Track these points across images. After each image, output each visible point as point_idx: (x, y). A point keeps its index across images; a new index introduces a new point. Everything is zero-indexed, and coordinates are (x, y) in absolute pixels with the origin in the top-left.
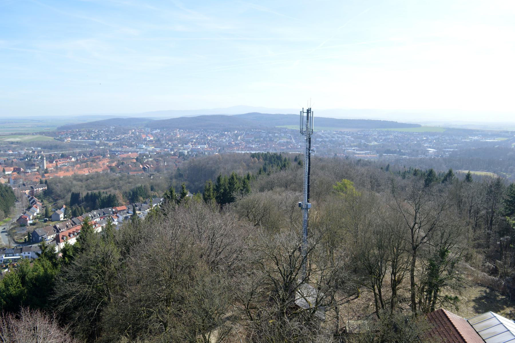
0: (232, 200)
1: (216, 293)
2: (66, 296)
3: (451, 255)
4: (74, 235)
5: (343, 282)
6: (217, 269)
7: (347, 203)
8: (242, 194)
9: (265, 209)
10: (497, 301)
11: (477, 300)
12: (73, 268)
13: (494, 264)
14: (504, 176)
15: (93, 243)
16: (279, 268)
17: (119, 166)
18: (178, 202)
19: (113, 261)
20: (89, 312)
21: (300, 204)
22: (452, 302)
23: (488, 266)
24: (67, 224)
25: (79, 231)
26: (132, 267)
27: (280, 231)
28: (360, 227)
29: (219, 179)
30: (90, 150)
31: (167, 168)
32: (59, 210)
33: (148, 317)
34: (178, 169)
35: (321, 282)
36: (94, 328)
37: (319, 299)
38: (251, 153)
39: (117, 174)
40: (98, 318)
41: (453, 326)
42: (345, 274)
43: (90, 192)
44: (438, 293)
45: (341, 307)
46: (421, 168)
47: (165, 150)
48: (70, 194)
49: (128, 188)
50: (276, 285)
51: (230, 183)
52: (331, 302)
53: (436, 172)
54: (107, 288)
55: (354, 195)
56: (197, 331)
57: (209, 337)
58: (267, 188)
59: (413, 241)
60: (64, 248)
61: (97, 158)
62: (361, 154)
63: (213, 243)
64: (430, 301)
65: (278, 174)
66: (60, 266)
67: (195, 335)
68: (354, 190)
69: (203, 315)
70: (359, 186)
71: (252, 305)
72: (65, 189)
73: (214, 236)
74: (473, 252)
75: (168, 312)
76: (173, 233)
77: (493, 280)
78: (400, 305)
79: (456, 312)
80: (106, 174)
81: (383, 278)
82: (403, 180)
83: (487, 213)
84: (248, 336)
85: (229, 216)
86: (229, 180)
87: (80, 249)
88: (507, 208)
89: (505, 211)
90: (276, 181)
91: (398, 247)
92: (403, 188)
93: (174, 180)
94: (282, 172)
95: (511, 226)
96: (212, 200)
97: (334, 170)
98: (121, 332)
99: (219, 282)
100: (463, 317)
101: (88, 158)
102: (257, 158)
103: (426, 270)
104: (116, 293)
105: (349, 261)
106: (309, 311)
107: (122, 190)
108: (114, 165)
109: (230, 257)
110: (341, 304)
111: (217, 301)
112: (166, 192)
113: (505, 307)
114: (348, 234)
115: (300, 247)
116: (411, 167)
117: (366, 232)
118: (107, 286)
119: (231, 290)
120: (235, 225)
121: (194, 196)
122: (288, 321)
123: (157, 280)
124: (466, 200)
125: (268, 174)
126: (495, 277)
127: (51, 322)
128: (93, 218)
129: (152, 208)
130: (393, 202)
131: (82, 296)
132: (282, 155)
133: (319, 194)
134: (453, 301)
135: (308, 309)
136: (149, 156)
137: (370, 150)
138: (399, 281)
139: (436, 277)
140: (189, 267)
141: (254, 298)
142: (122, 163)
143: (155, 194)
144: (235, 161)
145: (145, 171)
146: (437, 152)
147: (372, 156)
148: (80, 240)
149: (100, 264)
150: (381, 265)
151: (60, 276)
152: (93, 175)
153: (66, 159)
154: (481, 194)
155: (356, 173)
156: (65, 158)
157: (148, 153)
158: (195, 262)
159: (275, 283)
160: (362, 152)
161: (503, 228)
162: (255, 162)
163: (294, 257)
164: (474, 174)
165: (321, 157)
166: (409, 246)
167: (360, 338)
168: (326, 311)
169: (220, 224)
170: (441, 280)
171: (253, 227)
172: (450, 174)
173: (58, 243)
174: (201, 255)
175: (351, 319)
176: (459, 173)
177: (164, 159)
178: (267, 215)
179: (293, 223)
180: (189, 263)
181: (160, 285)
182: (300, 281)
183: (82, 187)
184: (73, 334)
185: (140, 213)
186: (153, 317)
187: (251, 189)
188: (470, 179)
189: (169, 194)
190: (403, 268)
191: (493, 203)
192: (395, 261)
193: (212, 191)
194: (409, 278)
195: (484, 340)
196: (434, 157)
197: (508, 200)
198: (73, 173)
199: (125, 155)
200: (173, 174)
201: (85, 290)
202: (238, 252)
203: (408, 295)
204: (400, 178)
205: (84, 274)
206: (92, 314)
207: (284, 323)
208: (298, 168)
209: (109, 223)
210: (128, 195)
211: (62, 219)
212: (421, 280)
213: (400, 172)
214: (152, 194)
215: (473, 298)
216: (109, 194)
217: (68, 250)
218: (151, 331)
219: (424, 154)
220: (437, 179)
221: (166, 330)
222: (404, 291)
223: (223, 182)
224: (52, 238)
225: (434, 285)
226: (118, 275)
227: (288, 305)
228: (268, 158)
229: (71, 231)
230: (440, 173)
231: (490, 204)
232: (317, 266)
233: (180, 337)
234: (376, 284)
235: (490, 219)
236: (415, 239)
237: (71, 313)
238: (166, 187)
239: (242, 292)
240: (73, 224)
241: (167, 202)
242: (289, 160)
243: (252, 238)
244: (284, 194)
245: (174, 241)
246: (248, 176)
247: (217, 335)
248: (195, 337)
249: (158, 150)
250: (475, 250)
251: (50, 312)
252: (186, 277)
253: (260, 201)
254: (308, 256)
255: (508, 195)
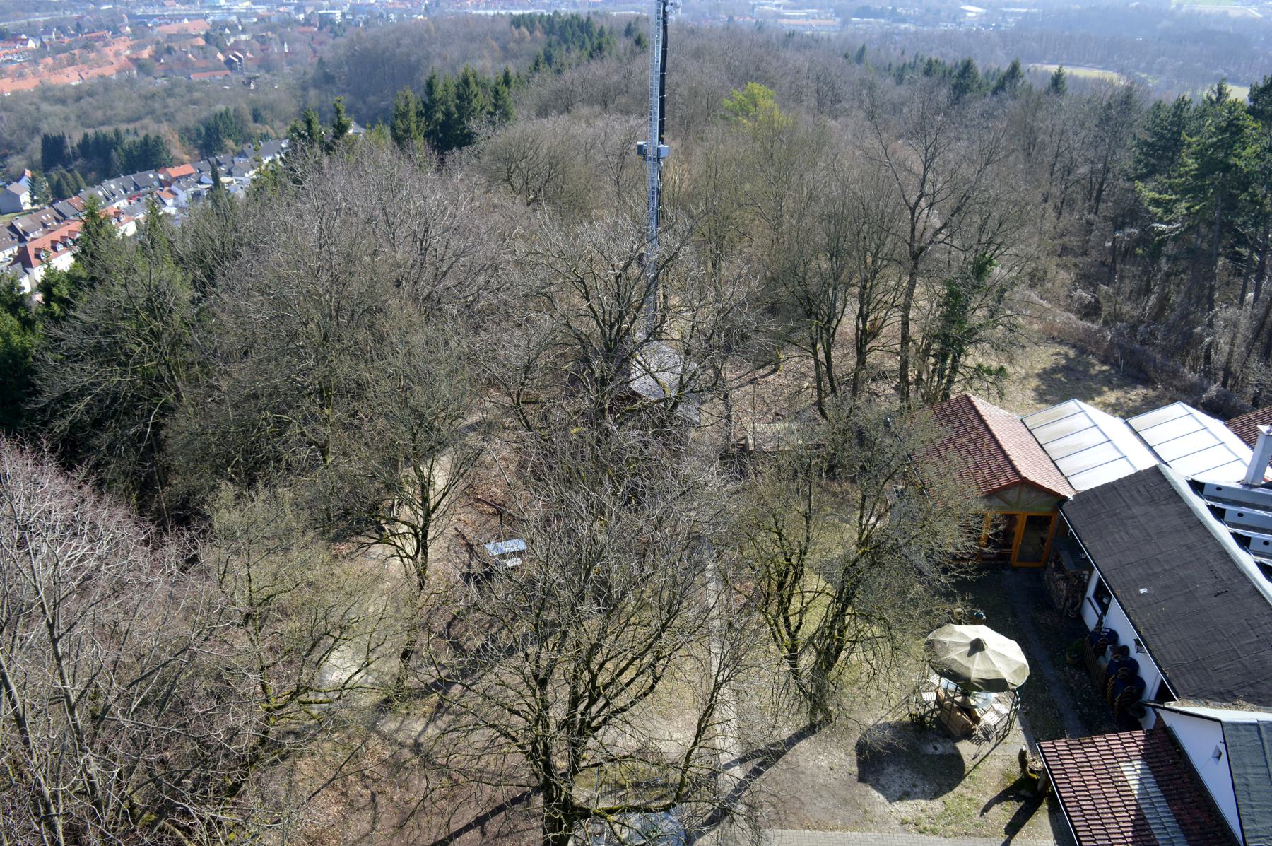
0: (466, 139)
1: (441, 371)
2: (67, 398)
3: (997, 272)
4: (65, 245)
5: (744, 337)
6: (439, 314)
7: (758, 144)
8: (493, 123)
9: (553, 162)
10: (1090, 375)
11: (1045, 375)
12: (75, 328)
13: (1094, 292)
14: (1144, 82)
15: (116, 262)
16: (590, 306)
17: (160, 57)
18: (329, 149)
19: (176, 305)
20: (133, 430)
21: (640, 147)
22: (991, 379)
23: (1080, 298)
24: (44, 217)
25: (78, 235)
26: (224, 317)
27: (590, 216)
28: (789, 203)
29: (430, 86)
30: (75, 15)
31: (291, 58)
32: (14, 183)
33: (280, 434)
34: (321, 62)
35: (691, 337)
36: (151, 466)
37: (686, 377)
38: (511, 14)
39: (159, 81)
40: (157, 444)
41: (990, 432)
42: (748, 317)
43: (91, 132)
44: (962, 359)
45: (736, 394)
46: (942, 55)
47: (281, 9)
48: (37, 143)
49: (192, 116)
50: (584, 347)
51: (459, 97)
52: (716, 383)
53: (979, 67)
54: (170, 371)
55: (776, 125)
56: (401, 459)
57: (430, 472)
58: (555, 108)
59: (913, 237)
60: (44, 281)
61: (99, 38)
62: (794, 17)
63: (426, 249)
64: (941, 376)
65: (582, 69)
66: (41, 326)
67: (396, 470)
68: (776, 112)
69: (411, 422)
70: (786, 103)
71: (528, 394)
72: (23, 126)
73: (426, 231)
74: (1051, 264)
75: (326, 420)
76: (321, 228)
77: (1087, 330)
78: (873, 386)
79: (998, 400)
80: (127, 80)
81: (837, 326)
82: (898, 88)
83: (1092, 172)
84: (522, 465)
85: (462, 180)
86: (458, 87)
87: (85, 279)
88: (1139, 161)
89: (1136, 169)
90: (579, 89)
91: (877, 253)
92: (896, 109)
93: (312, 93)
94: (594, 65)
95: (1142, 205)
96: (415, 142)
97: (727, 59)
98: (218, 471)
99: (447, 343)
100: (1012, 411)
101: (72, 39)
102: (527, 27)
103: (939, 306)
104: (193, 381)
105: (759, 286)
106: (662, 405)
107: (177, 122)
108: (145, 54)
109: (470, 283)
110: (737, 388)
111: (444, 389)
112: (293, 123)
113: (1105, 389)
114: (756, 222)
115: (642, 254)
116: (920, 54)
117: (802, 216)
118: (168, 366)
119: (476, 362)
120: (477, 204)
121: (368, 131)
122: (615, 428)
123: (291, 346)
124: (1047, 138)
125: (559, 72)
126: (1093, 322)
127: (38, 462)
128: (108, 199)
129: (263, 168)
130: (871, 142)
131: (108, 394)
132: (593, 19)
133: (686, 123)
134: (993, 377)
135: (661, 401)
136: (240, 28)
137: (820, 8)
138: (874, 334)
139: (960, 322)
140: (372, 311)
141: (533, 379)
142: (169, 50)
143: (264, 131)
144: (471, 38)
145: (231, 69)
146: (986, 14)
147: (823, 22)
148: (82, 256)
149: (143, 315)
150: (835, 295)
151: (46, 349)
152: (91, 85)
153: (12, 44)
154: (1082, 125)
155: (781, 67)
156: (9, 40)
157: (234, 18)
158: (382, 298)
159: (582, 341)
160: (797, 13)
161: (1123, 209)
162: (522, 39)
163: (627, 278)
164: (1071, 74)
165: (694, 24)
166: (903, 251)
167: (781, 462)
168: (703, 403)
169: (440, 202)
170: (969, 331)
171: (522, 209)
172: (1014, 72)
173: (28, 269)
174: (398, 281)
175: (759, 420)
176: (1036, 71)
177: (280, 36)
178: (556, 176)
179: (624, 195)
180: (369, 302)
181: (301, 359)
182: (640, 336)
183: (66, 119)
184: (100, 483)
185: (232, 182)
186: (293, 432)
187: (514, 111)
188: (1060, 86)
189: (302, 127)
190: (886, 303)
191: (1109, 148)
192: (868, 285)
193: (414, 118)
194: (898, 325)
195: (1053, 462)
196: (978, 29)
197: (1145, 143)
198: (36, 82)
199: (173, 28)
200: (309, 76)
201: (116, 379)
202: (489, 271)
203: (892, 364)
204: (890, 81)
205: (105, 342)
206: (141, 436)
207: (607, 433)
208: (634, 54)
209: (154, 212)
210: (194, 136)
211: (27, 207)
212: (923, 330)
213: (890, 65)
214: (259, 131)
215: (1038, 368)
216: (142, 134)
217: (55, 284)
218: (289, 465)
219: (954, 20)
220: (980, 87)
221: (325, 461)
222: (883, 357)
223: (441, 93)
224: (10, 256)
225: (954, 342)
226: (193, 340)
227: (616, 392)
228: (557, 27)
229: (56, 236)
230: (988, 71)
231: (1102, 149)
232: (683, 300)
233: (360, 475)
234: (819, 340)
235: (1097, 187)
236: (917, 234)
237: (89, 437)
238: (293, 110)
239: (504, 366)
240: (60, 217)
241: (299, 148)
242: (611, 32)
243: (522, 236)
244: (599, 123)
245: (326, 247)
246: (506, 75)
247: (448, 466)
248: (397, 473)
249: (261, 10)
250: (1055, 260)
251: (34, 439)
252: (362, 335)
253: (538, 142)
254: (660, 277)
255: (1148, 129)
